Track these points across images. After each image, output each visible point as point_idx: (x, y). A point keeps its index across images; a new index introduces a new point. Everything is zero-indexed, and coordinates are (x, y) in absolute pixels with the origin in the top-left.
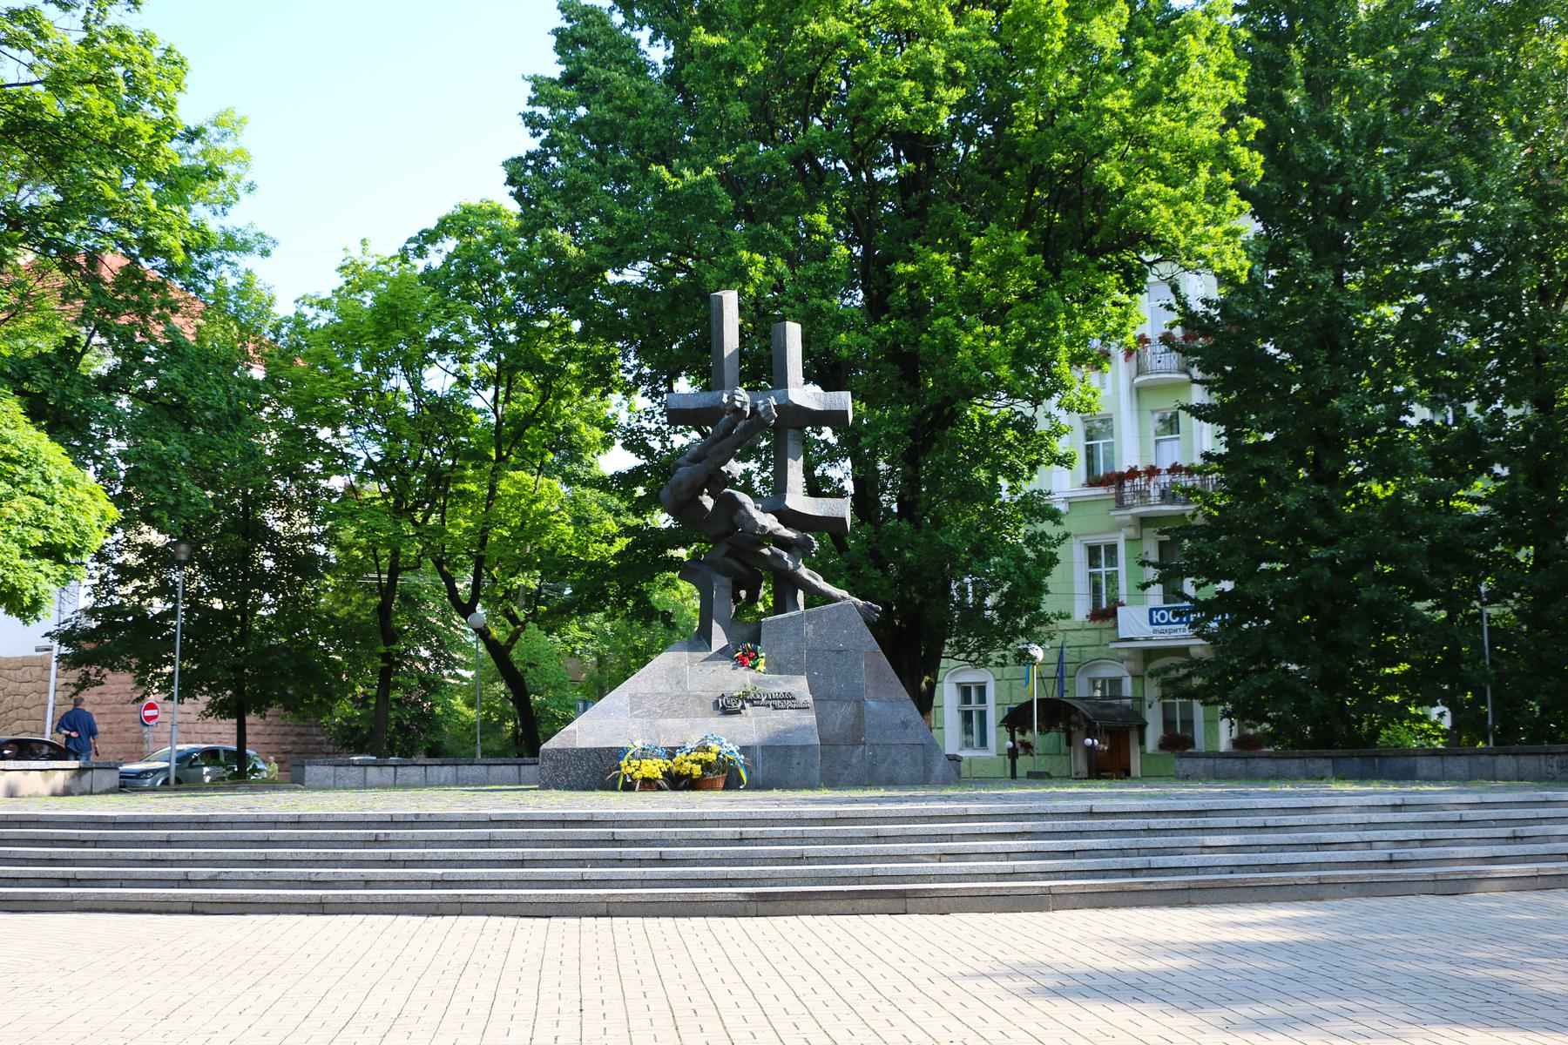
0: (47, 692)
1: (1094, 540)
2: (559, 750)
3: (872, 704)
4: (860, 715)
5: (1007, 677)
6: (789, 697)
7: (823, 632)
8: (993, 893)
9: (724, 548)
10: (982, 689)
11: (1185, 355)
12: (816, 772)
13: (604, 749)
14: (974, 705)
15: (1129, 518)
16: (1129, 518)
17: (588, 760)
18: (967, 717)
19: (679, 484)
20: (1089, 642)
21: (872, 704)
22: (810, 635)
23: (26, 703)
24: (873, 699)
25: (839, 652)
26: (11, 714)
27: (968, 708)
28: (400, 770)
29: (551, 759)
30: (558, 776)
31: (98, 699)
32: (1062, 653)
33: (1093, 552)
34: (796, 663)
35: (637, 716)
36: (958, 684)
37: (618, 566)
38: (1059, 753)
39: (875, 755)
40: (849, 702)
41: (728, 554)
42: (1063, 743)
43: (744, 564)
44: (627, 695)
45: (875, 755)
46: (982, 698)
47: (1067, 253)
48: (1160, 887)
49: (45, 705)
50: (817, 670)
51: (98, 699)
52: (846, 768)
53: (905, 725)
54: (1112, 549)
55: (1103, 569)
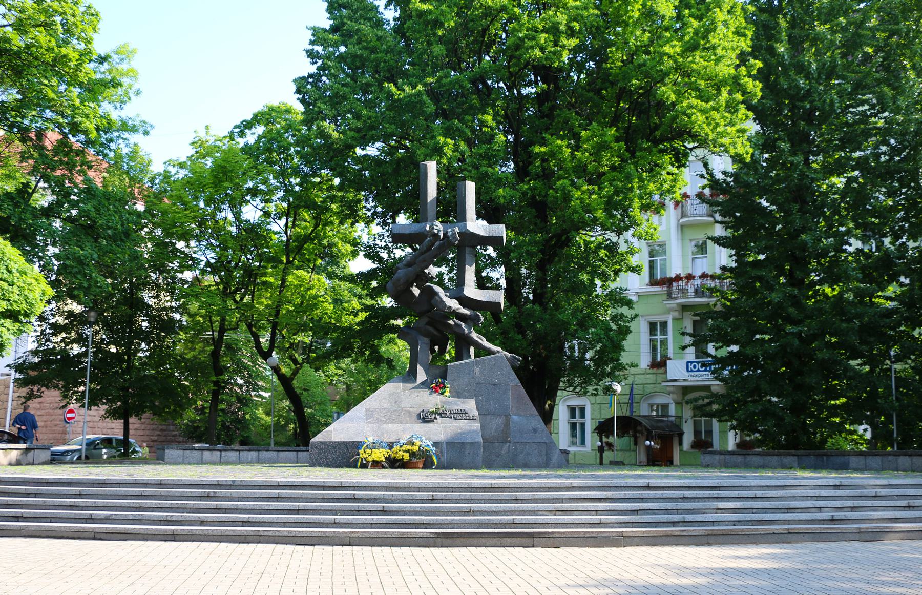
0: (7, 401)
1: (653, 319)
3: (514, 417)
4: (507, 424)
7: (485, 372)
8: (587, 535)
9: (425, 320)
10: (582, 410)
12: (480, 459)
13: (349, 442)
14: (578, 419)
15: (675, 305)
17: (339, 449)
18: (573, 426)
19: (398, 280)
20: (649, 381)
22: (478, 373)
24: (515, 414)
25: (495, 385)
27: (574, 421)
28: (223, 453)
29: (316, 448)
30: (321, 459)
31: (38, 406)
32: (632, 388)
33: (653, 326)
34: (469, 391)
35: (370, 422)
36: (568, 406)
38: (630, 450)
39: (516, 449)
40: (501, 416)
41: (428, 324)
43: (438, 330)
44: (364, 410)
45: (516, 449)
46: (583, 415)
48: (690, 533)
49: (6, 409)
50: (481, 396)
52: (498, 457)
53: (535, 430)
54: (664, 325)
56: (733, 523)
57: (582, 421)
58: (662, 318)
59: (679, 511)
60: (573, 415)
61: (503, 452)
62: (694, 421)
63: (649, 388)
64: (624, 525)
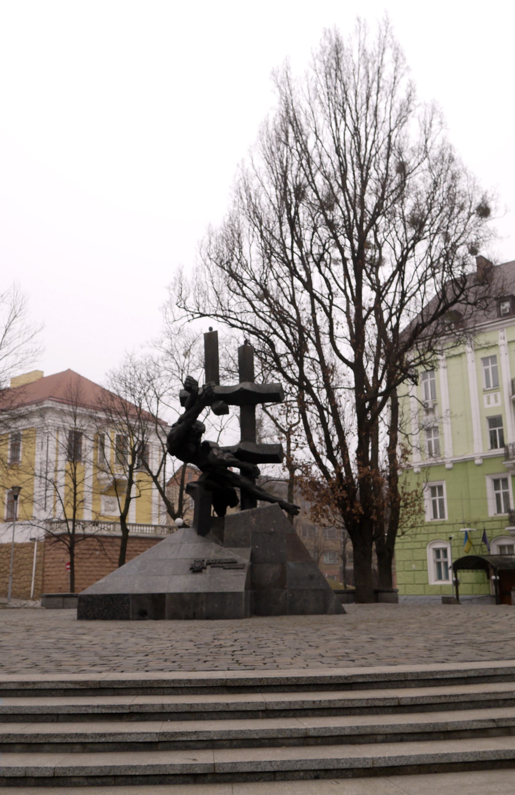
0: (33, 558)
1: (496, 477)
2: (89, 596)
4: (283, 572)
5: (457, 544)
6: (234, 562)
10: (445, 551)
11: (389, 478)
14: (442, 559)
15: (512, 465)
16: (512, 465)
18: (439, 564)
20: (496, 527)
21: (291, 565)
23: (26, 563)
25: (271, 533)
26: (21, 568)
27: (439, 560)
31: (51, 560)
32: (484, 534)
33: (496, 482)
36: (434, 549)
37: (365, 256)
38: (484, 583)
42: (486, 577)
46: (446, 556)
47: (326, 486)
49: (32, 563)
51: (51, 560)
54: (505, 480)
55: (501, 491)
56: (315, 774)
57: (445, 560)
58: (503, 476)
59: (235, 743)
60: (438, 556)
61: (280, 599)
62: (11, 597)
63: (496, 533)
64: (99, 781)
